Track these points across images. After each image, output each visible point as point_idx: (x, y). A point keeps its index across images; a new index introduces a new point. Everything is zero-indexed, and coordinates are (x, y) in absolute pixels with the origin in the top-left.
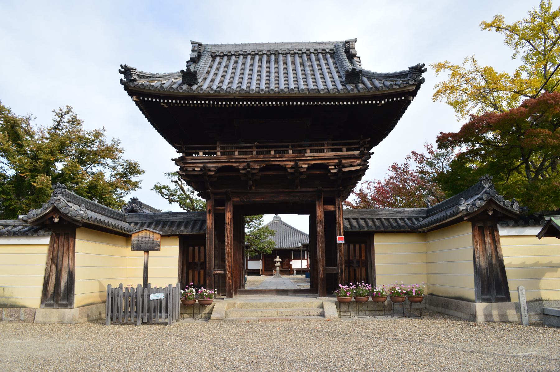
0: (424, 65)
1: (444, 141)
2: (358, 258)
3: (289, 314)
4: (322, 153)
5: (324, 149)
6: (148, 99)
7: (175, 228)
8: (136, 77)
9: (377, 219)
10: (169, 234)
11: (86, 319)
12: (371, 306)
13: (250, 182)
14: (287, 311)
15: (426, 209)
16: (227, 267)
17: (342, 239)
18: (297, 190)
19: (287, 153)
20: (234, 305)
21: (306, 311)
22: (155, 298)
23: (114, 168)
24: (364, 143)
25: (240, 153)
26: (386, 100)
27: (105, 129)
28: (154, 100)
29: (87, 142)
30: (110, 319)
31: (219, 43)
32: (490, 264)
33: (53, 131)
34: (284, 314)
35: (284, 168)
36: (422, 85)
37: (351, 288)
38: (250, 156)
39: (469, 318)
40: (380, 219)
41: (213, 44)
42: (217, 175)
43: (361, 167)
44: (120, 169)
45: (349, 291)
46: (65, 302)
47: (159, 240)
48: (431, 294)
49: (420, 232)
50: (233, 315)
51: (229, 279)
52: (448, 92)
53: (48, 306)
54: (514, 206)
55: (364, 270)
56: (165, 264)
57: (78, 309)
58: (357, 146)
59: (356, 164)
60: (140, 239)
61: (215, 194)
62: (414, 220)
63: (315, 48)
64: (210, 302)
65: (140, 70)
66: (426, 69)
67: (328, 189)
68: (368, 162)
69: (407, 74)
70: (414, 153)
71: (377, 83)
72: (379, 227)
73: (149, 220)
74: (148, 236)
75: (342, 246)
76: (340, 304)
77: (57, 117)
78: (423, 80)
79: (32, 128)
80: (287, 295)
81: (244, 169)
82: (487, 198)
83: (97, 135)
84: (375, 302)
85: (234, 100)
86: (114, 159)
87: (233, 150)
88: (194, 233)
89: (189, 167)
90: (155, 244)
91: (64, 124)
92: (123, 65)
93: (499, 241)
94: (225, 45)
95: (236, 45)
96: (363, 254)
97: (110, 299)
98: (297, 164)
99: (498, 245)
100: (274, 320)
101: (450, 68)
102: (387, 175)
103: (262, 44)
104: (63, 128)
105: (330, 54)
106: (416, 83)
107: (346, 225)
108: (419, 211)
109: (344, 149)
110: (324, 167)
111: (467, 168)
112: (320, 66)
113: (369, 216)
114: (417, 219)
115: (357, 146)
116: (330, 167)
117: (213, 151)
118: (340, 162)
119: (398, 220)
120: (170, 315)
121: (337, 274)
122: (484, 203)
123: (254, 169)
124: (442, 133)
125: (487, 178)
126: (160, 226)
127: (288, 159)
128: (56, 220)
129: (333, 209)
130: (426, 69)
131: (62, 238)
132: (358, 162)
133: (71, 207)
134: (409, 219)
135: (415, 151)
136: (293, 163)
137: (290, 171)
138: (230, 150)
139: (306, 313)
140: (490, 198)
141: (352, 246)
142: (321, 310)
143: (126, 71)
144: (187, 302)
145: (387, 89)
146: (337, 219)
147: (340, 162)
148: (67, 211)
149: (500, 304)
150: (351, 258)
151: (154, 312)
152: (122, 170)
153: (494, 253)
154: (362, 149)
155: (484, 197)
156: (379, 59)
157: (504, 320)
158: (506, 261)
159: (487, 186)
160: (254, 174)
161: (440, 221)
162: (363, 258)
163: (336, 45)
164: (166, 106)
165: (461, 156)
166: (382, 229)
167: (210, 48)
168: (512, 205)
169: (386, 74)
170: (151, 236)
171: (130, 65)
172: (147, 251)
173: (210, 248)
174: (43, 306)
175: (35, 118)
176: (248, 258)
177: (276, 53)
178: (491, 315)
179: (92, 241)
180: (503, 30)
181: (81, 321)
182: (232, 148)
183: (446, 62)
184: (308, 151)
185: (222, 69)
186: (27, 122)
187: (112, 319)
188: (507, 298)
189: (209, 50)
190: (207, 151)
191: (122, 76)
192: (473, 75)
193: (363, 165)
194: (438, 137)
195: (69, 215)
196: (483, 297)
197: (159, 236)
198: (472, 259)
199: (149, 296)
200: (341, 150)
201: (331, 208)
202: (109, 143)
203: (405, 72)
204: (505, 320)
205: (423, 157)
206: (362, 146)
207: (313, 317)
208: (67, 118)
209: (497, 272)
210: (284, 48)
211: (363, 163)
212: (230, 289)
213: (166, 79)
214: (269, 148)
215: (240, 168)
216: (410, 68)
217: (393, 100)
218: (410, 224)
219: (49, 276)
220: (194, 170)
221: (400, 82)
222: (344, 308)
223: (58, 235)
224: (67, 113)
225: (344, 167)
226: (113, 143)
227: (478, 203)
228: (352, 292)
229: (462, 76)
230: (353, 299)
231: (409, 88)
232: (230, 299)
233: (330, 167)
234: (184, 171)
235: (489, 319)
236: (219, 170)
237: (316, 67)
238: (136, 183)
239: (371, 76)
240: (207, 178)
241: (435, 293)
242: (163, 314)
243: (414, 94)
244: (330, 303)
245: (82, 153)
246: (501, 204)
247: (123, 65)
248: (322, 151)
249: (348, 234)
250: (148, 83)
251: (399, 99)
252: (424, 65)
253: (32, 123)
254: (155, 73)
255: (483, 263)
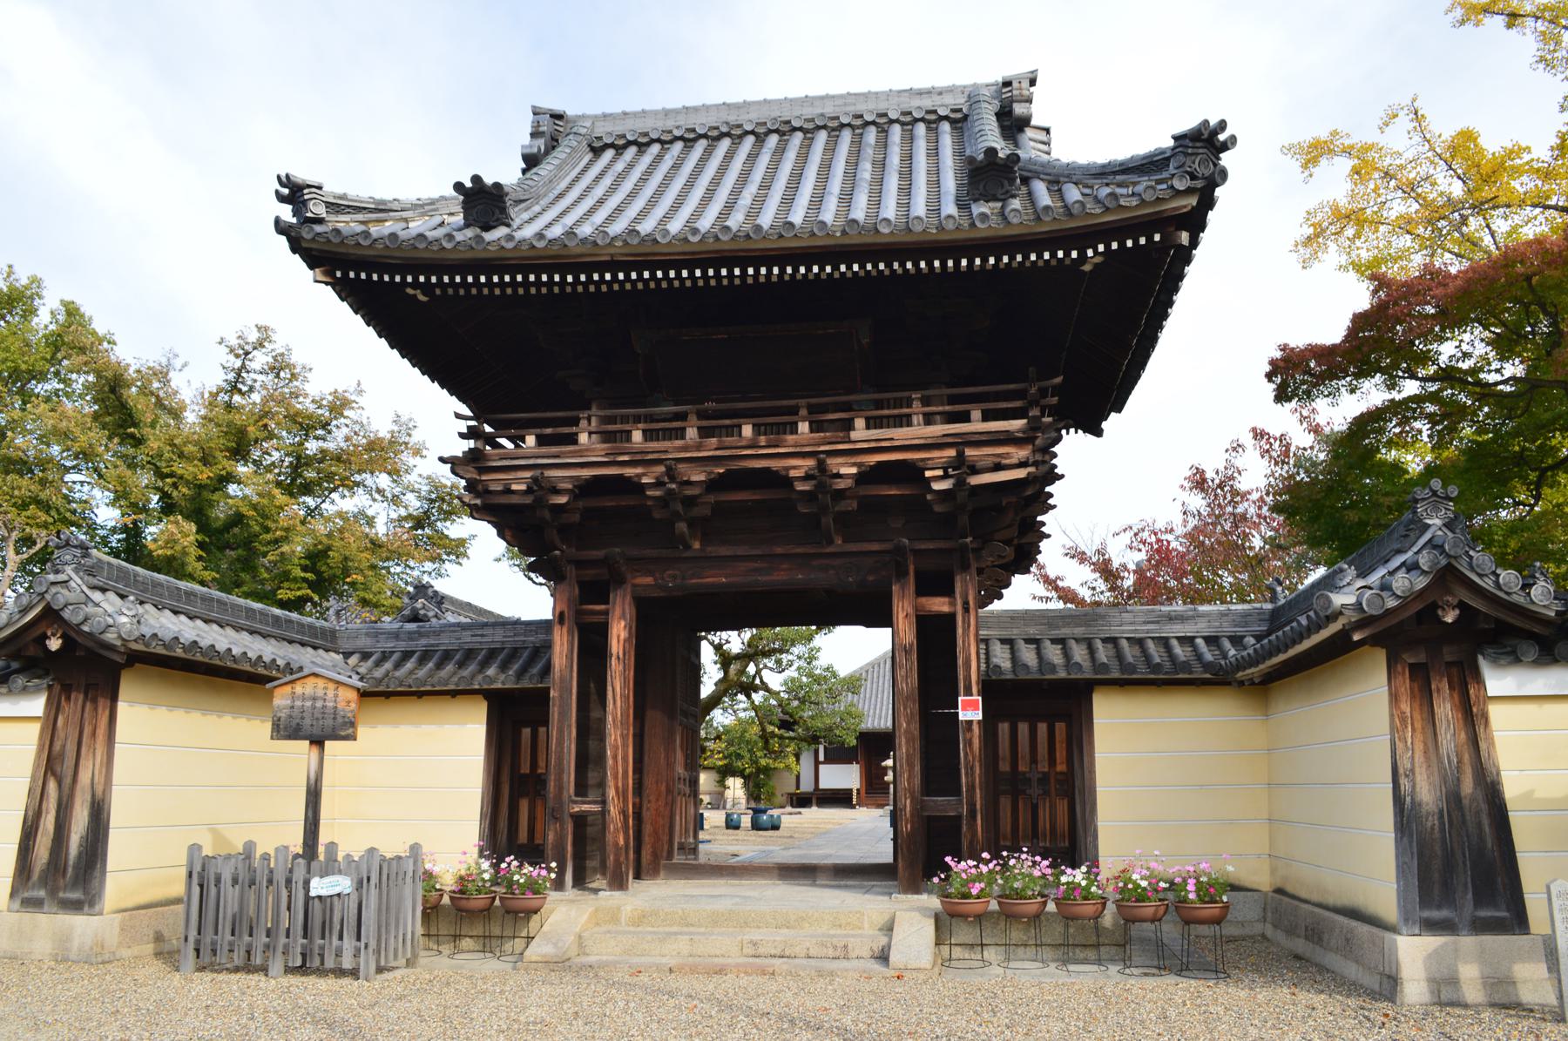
0: (1222, 125)
1: (1297, 373)
2: (1043, 767)
3: (778, 952)
4: (900, 430)
5: (909, 416)
6: (358, 275)
7: (472, 668)
8: (318, 209)
9: (1105, 640)
10: (452, 687)
11: (150, 948)
12: (1055, 931)
13: (682, 527)
14: (771, 939)
15: (1269, 606)
16: (611, 793)
17: (973, 705)
18: (828, 550)
19: (794, 431)
20: (614, 917)
21: (835, 941)
22: (324, 893)
23: (396, 500)
24: (1043, 393)
25: (649, 435)
26: (1101, 248)
27: (363, 387)
28: (386, 278)
29: (307, 425)
30: (191, 954)
31: (618, 110)
32: (1453, 798)
33: (224, 397)
34: (761, 950)
35: (781, 481)
36: (1218, 192)
37: (984, 869)
38: (679, 443)
39: (1377, 987)
40: (1112, 641)
41: (599, 112)
42: (581, 504)
43: (1032, 469)
44: (414, 504)
45: (980, 877)
46: (75, 895)
47: (353, 705)
48: (1279, 891)
49: (1241, 683)
50: (603, 950)
51: (616, 830)
52: (1350, 232)
53: (33, 904)
54: (1536, 592)
55: (1062, 806)
56: (420, 786)
57: (119, 916)
58: (1018, 404)
59: (1014, 461)
60: (298, 703)
61: (580, 564)
62: (1227, 644)
63: (906, 108)
64: (534, 904)
65: (339, 191)
66: (1233, 139)
67: (931, 546)
68: (1055, 455)
69: (1168, 159)
70: (1258, 434)
71: (1073, 194)
72: (1104, 667)
73: (402, 645)
74: (320, 693)
75: (976, 728)
76: (944, 925)
77: (231, 357)
78: (1223, 174)
79: (176, 392)
80: (814, 885)
81: (659, 484)
82: (1434, 563)
83: (339, 405)
84: (1067, 917)
85: (613, 265)
86: (394, 473)
87: (627, 427)
88: (526, 684)
89: (495, 481)
90: (340, 720)
91: (252, 375)
92: (283, 175)
93: (1485, 717)
94: (635, 115)
95: (667, 113)
96: (1061, 754)
97: (196, 890)
98: (821, 466)
99: (1481, 731)
100: (721, 971)
101: (1347, 151)
102: (1178, 504)
103: (746, 105)
104: (251, 389)
105: (953, 122)
106: (1199, 184)
107: (995, 660)
108: (1245, 615)
109: (976, 414)
110: (911, 473)
111: (1384, 463)
112: (908, 158)
113: (1079, 631)
114: (1237, 641)
115: (1018, 404)
116: (928, 474)
117: (566, 430)
118: (961, 454)
119: (1174, 643)
120: (366, 946)
121: (959, 818)
122: (1421, 582)
123: (689, 483)
124: (1284, 348)
125: (1435, 493)
126: (431, 665)
127: (796, 450)
128: (54, 644)
129: (946, 609)
130: (1233, 139)
131: (76, 700)
132: (1021, 453)
133: (97, 605)
134: (1212, 640)
135: (1260, 426)
136: (811, 462)
137: (800, 487)
138: (618, 427)
139: (835, 948)
140: (1444, 562)
141: (1004, 728)
142: (884, 940)
143: (294, 192)
144: (464, 904)
145: (1099, 211)
146: (960, 642)
147: (961, 454)
148: (80, 618)
149: (1489, 940)
150: (1022, 768)
151: (323, 938)
152: (418, 504)
153: (1466, 757)
154: (1035, 412)
155: (1421, 562)
156: (1094, 125)
157: (1506, 1003)
158: (1512, 788)
159: (1438, 522)
160: (690, 502)
161: (1287, 648)
162: (1061, 767)
163: (973, 97)
164: (422, 298)
165: (1367, 423)
166: (1116, 675)
167: (588, 124)
168: (1526, 587)
169: (1104, 166)
170: (331, 693)
171: (302, 174)
172: (318, 742)
173: (561, 731)
174: (17, 905)
175: (185, 365)
176: (821, 758)
177: (786, 128)
178: (1453, 981)
179: (188, 708)
180: (1530, 22)
181: (125, 953)
182: (847, 407)
183: (1334, 133)
184: (860, 423)
185: (607, 181)
186: (162, 374)
187: (197, 951)
188: (1516, 920)
189: (583, 131)
190: (549, 431)
191: (286, 213)
192: (1424, 169)
193: (1035, 464)
194: (1272, 362)
195: (86, 628)
196: (1426, 914)
197: (353, 695)
198: (1390, 779)
199: (307, 883)
200: (965, 417)
201: (939, 605)
202: (382, 428)
203: (1162, 152)
204: (1504, 1000)
205: (1288, 446)
206: (1034, 403)
207: (855, 963)
208: (260, 360)
209: (1479, 825)
210: (809, 112)
211: (1039, 457)
212: (618, 864)
213: (423, 214)
214: (743, 421)
215: (645, 480)
216: (1176, 138)
217: (1122, 244)
218: (1209, 657)
219: (38, 814)
220: (508, 491)
221: (1144, 183)
222: (965, 933)
223: (67, 690)
224: (260, 345)
225: (975, 471)
226: (396, 428)
227: (1401, 582)
228: (989, 884)
229: (1387, 175)
230: (994, 905)
231: (1174, 204)
232: (617, 894)
233: (928, 474)
234: (478, 495)
235: (1445, 994)
236: (586, 489)
237: (895, 159)
238: (462, 542)
239: (1057, 177)
240: (547, 515)
241: (1289, 889)
242: (348, 944)
243: (1196, 222)
244: (916, 915)
245: (301, 461)
246: (1487, 584)
247: (283, 175)
248: (905, 421)
249: (995, 691)
250: (360, 228)
251: (1143, 241)
252: (1222, 125)
253: (176, 380)
254: (388, 196)
255: (1426, 792)
